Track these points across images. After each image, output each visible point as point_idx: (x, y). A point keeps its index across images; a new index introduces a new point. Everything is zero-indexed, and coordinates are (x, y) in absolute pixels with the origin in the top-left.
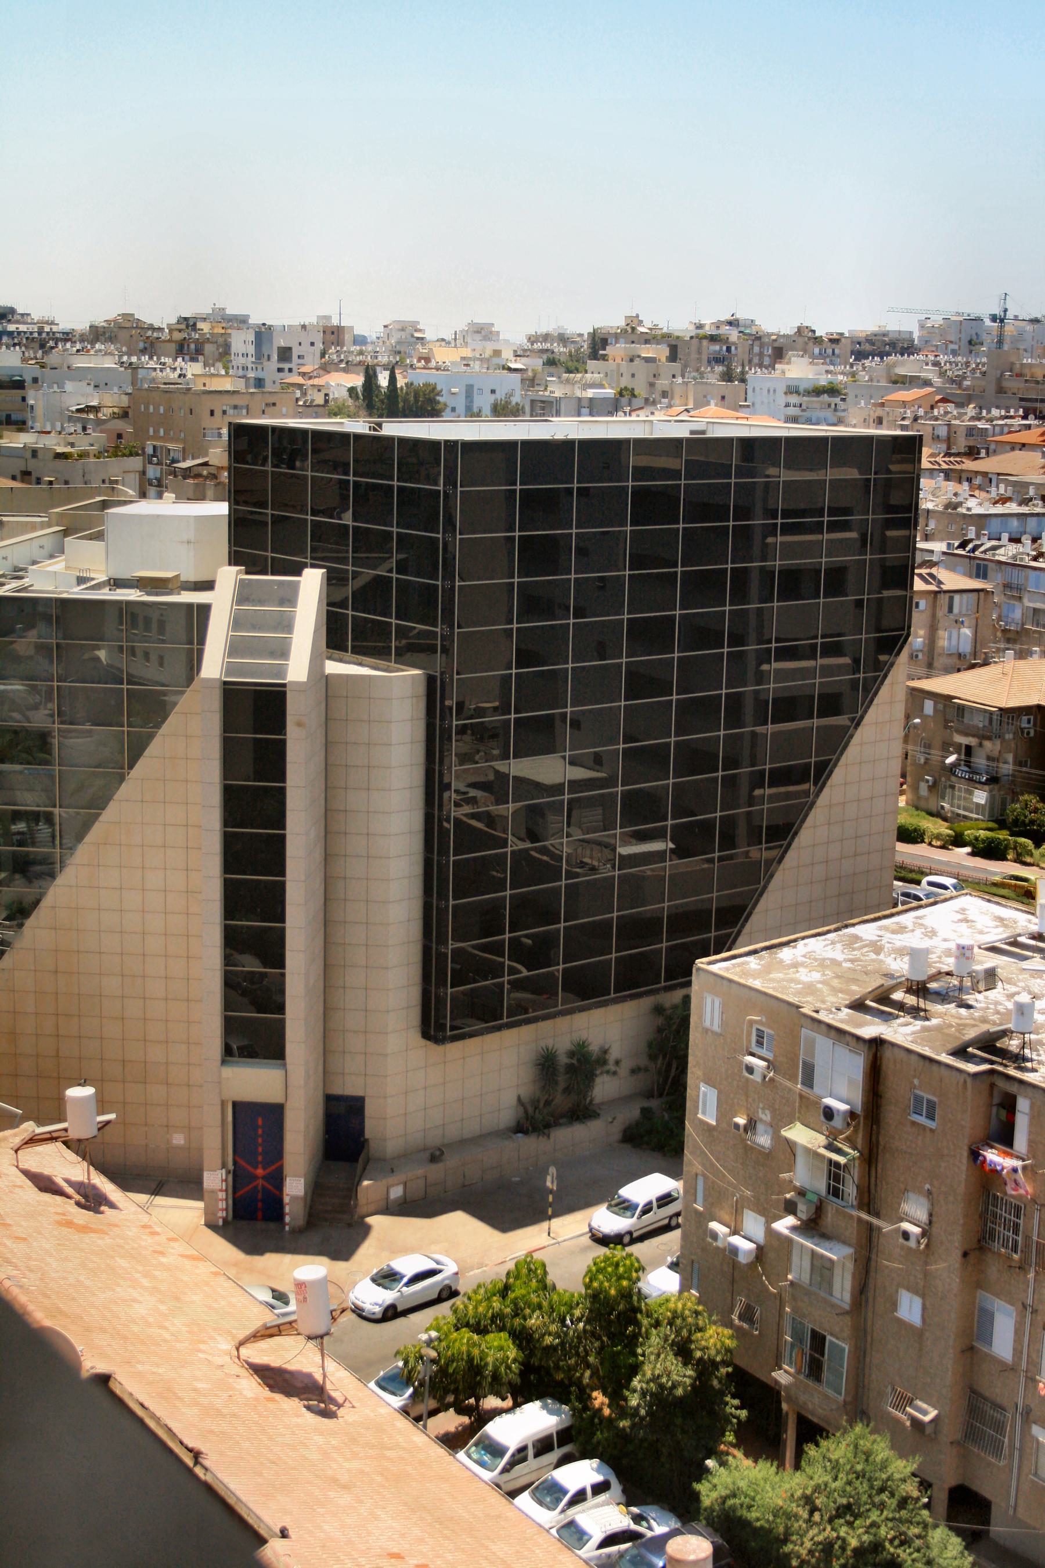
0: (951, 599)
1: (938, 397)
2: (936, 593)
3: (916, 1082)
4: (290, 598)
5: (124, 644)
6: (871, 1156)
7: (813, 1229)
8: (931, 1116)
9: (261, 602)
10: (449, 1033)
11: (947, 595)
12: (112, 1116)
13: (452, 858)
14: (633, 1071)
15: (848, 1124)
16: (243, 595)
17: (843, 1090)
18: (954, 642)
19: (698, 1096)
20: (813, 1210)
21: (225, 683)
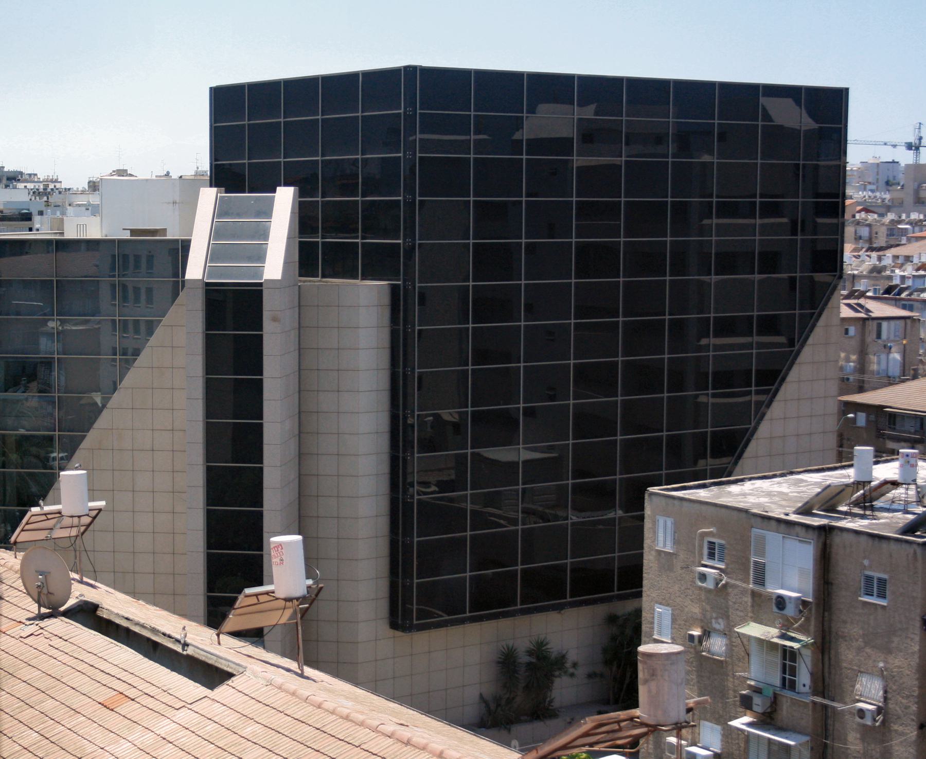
0: (879, 327)
1: (859, 208)
2: (864, 319)
3: (866, 562)
4: (267, 211)
5: (117, 318)
6: (824, 645)
7: (768, 724)
8: (882, 595)
9: (239, 215)
10: (415, 622)
11: (875, 322)
12: (101, 504)
13: (415, 581)
14: (590, 676)
15: (801, 612)
16: (221, 210)
17: (794, 578)
18: (883, 366)
19: (653, 618)
20: (768, 704)
21: (207, 284)
